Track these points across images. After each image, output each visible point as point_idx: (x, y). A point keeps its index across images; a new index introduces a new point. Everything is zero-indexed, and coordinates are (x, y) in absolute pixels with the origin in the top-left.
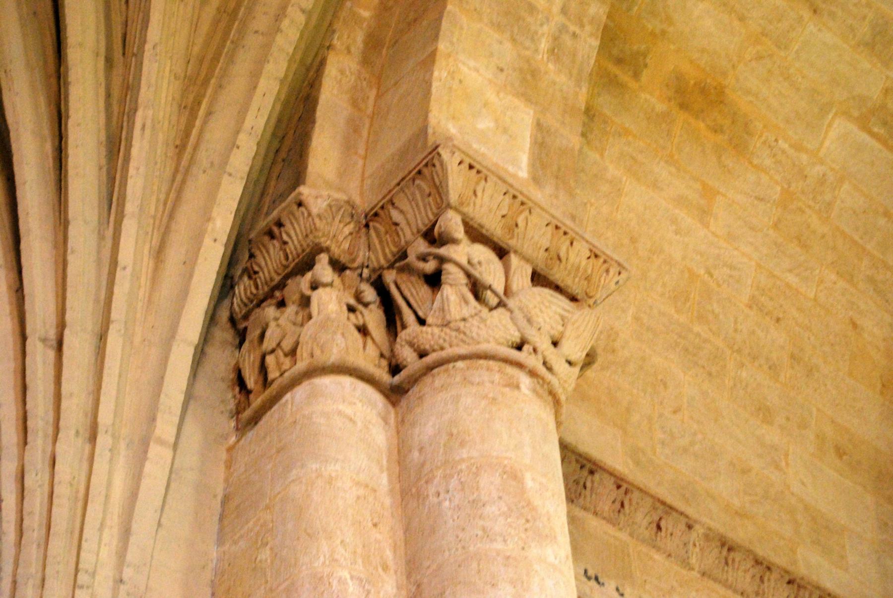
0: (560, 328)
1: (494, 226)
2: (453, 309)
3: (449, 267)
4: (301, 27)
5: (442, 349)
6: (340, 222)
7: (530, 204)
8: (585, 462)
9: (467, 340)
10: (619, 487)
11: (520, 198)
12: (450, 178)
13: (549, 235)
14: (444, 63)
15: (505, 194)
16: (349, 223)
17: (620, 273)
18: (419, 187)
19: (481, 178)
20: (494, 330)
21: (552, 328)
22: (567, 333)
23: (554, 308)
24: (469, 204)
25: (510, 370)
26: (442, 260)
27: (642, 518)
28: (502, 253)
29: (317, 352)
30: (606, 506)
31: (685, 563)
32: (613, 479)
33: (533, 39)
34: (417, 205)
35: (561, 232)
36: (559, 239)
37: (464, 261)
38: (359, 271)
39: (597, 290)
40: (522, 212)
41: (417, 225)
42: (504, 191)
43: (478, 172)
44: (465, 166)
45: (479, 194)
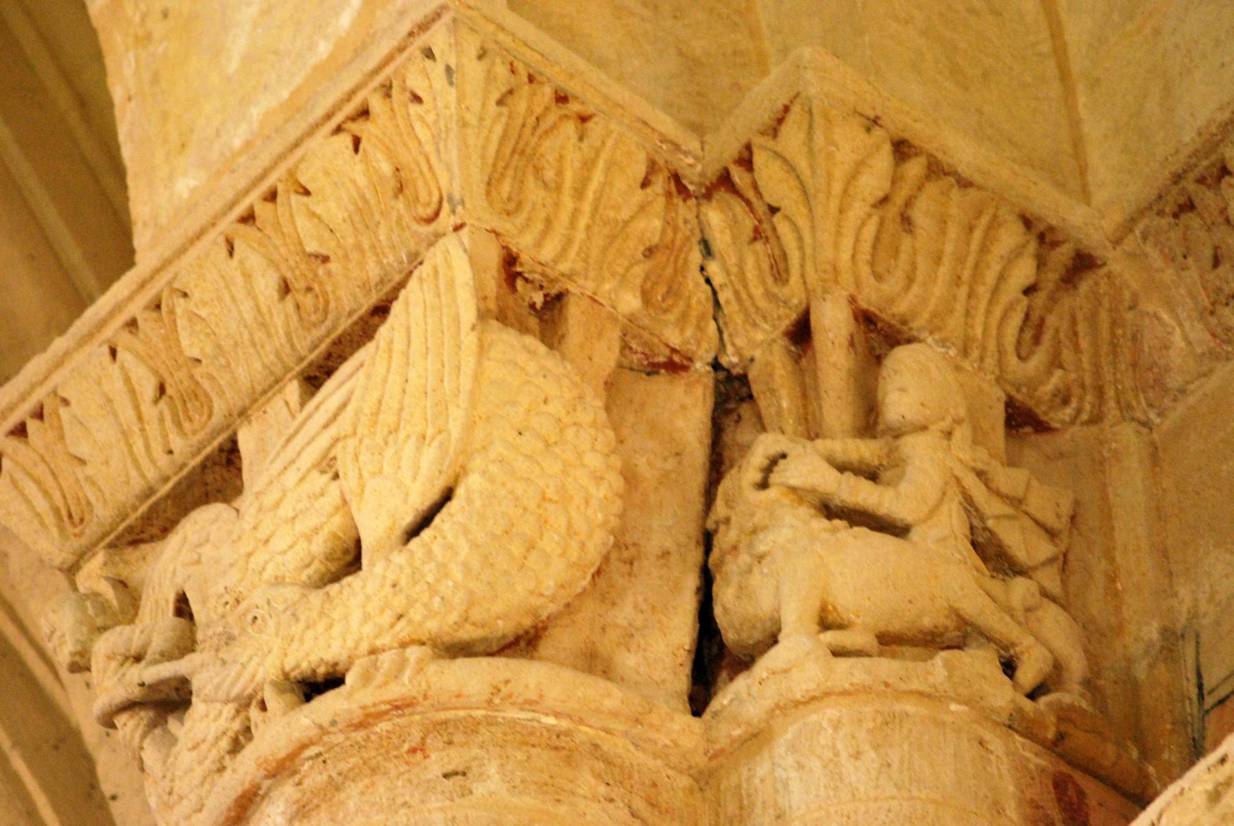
11: (254, 198)
15: (113, 352)
17: (429, 54)
23: (291, 477)
36: (277, 225)
43: (39, 415)
45: (83, 450)
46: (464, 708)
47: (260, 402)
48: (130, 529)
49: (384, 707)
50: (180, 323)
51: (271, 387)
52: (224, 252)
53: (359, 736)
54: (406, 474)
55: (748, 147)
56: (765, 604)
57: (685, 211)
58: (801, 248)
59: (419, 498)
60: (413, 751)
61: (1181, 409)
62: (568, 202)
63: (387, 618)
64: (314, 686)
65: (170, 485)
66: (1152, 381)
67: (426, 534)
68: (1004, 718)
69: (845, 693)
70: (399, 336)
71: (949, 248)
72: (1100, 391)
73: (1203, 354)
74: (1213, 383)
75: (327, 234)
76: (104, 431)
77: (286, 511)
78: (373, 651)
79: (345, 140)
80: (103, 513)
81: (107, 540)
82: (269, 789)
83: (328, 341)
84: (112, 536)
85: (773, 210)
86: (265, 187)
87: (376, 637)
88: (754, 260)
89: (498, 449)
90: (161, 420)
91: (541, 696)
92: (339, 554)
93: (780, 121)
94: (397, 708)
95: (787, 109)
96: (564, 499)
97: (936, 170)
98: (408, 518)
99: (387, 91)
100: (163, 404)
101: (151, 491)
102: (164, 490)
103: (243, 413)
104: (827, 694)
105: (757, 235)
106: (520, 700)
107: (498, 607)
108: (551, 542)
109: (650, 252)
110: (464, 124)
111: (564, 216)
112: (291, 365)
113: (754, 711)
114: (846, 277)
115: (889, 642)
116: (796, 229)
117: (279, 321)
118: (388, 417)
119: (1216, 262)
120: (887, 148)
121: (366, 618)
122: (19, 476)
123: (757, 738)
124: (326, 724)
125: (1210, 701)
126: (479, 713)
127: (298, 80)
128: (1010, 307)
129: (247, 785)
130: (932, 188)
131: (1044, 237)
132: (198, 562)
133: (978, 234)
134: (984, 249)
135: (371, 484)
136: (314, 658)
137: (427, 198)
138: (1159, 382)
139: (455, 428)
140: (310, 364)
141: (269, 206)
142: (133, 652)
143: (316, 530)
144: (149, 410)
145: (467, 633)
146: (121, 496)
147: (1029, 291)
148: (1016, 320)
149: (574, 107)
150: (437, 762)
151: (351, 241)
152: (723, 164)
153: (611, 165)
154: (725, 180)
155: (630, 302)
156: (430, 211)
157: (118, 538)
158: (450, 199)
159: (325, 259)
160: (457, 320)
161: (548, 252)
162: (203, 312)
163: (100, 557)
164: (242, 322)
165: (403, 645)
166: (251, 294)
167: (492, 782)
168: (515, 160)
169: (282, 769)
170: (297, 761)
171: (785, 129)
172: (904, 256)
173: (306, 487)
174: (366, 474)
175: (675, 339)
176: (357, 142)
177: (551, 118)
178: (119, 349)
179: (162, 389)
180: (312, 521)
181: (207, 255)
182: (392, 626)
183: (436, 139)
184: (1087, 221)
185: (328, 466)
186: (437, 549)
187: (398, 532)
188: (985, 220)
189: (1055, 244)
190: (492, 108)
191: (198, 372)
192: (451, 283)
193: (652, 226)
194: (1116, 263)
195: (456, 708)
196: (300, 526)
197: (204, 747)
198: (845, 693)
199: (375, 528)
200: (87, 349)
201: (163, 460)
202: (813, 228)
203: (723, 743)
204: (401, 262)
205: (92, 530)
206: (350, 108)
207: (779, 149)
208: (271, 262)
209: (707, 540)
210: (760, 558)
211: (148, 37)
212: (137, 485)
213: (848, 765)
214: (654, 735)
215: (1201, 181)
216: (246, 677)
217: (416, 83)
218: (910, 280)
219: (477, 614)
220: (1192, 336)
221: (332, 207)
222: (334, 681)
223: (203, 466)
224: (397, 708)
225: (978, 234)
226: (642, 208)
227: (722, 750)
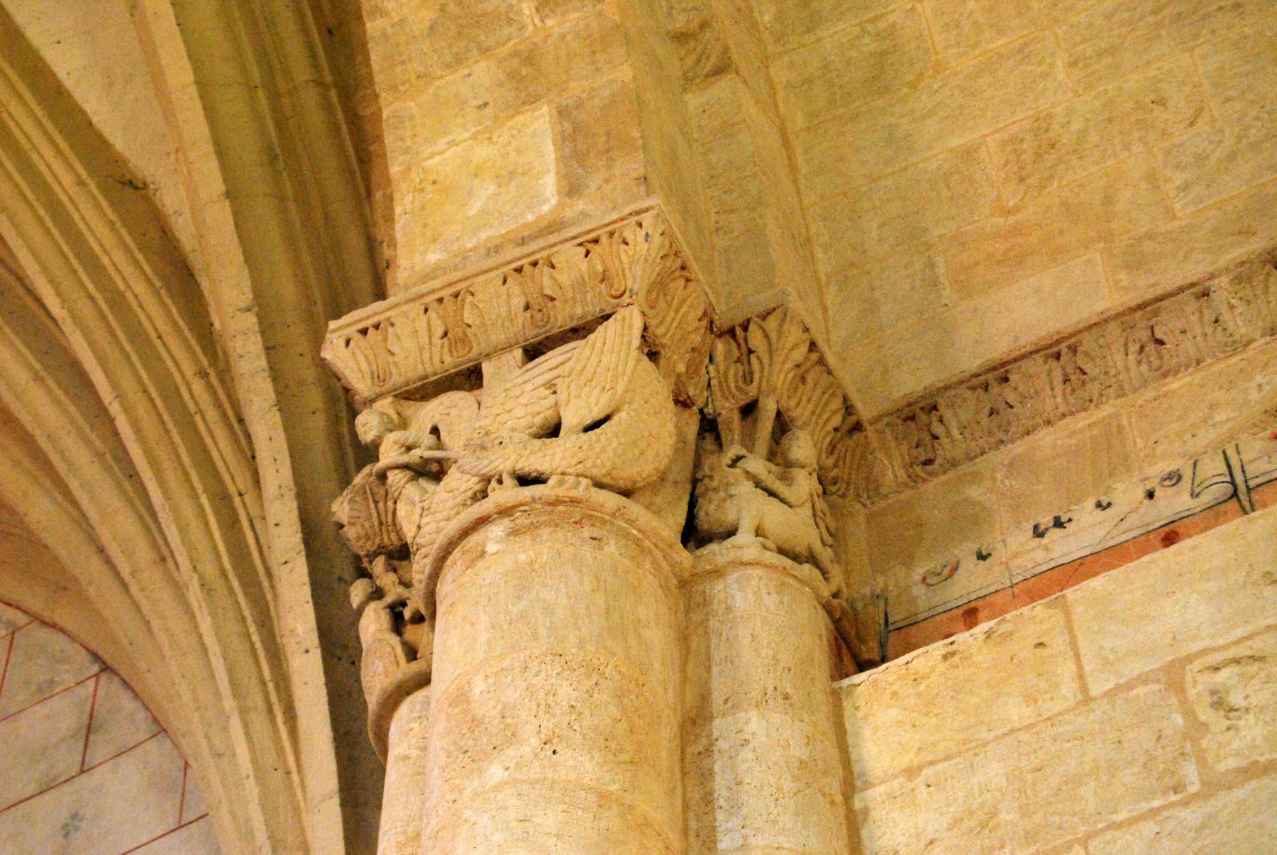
4: (257, 328)
7: (464, 285)
8: (1055, 349)
10: (1058, 356)
11: (446, 293)
14: (404, 186)
15: (426, 310)
17: (640, 225)
23: (529, 387)
27: (1119, 358)
30: (1055, 400)
31: (1237, 345)
32: (1039, 358)
33: (510, 21)
36: (532, 278)
42: (423, 308)
43: (377, 327)
45: (395, 349)
48: (407, 392)
50: (467, 307)
52: (501, 282)
53: (549, 508)
54: (593, 400)
55: (748, 321)
56: (731, 517)
57: (709, 338)
58: (762, 372)
59: (597, 414)
60: (576, 523)
61: (883, 504)
62: (672, 314)
63: (574, 461)
64: (524, 480)
66: (873, 488)
67: (598, 431)
68: (824, 601)
69: (766, 566)
70: (600, 340)
71: (814, 398)
72: (848, 484)
74: (902, 497)
76: (409, 343)
77: (523, 400)
78: (563, 474)
79: (582, 250)
80: (397, 379)
85: (750, 352)
86: (532, 259)
88: (735, 371)
89: (635, 405)
90: (442, 347)
93: (769, 314)
95: (774, 309)
96: (658, 439)
97: (821, 361)
98: (588, 421)
99: (611, 234)
100: (445, 340)
101: (426, 377)
102: (431, 379)
103: (488, 356)
104: (757, 564)
105: (738, 360)
107: (623, 475)
108: (650, 454)
109: (693, 349)
110: (646, 261)
111: (669, 319)
113: (720, 560)
114: (778, 391)
115: (781, 551)
116: (761, 363)
117: (520, 320)
118: (588, 374)
119: (917, 446)
120: (808, 344)
121: (563, 459)
122: (357, 351)
123: (717, 573)
125: (891, 627)
126: (607, 517)
127: (512, 227)
128: (828, 433)
130: (818, 368)
131: (848, 409)
132: (448, 414)
133: (826, 396)
134: (826, 404)
135: (574, 401)
136: (533, 468)
137: (618, 287)
138: (876, 489)
139: (620, 388)
143: (538, 414)
144: (437, 342)
145: (607, 480)
147: (836, 430)
148: (828, 440)
149: (686, 273)
150: (586, 532)
151: (570, 295)
153: (692, 306)
154: (731, 332)
155: (681, 368)
158: (631, 291)
159: (553, 299)
160: (630, 343)
161: (659, 332)
162: (481, 305)
163: (390, 399)
164: (499, 315)
165: (578, 475)
166: (508, 304)
167: (611, 548)
168: (659, 286)
169: (505, 512)
171: (771, 318)
172: (799, 393)
173: (537, 393)
175: (691, 392)
177: (677, 274)
179: (446, 334)
180: (537, 409)
183: (631, 263)
184: (865, 411)
185: (552, 387)
186: (603, 438)
188: (830, 391)
189: (851, 414)
190: (658, 260)
191: (468, 331)
192: (631, 327)
193: (697, 339)
194: (870, 431)
196: (529, 409)
197: (456, 493)
198: (766, 566)
199: (571, 419)
200: (412, 305)
201: (437, 365)
202: (771, 365)
203: (700, 569)
205: (389, 385)
206: (591, 236)
208: (524, 293)
209: (695, 482)
210: (731, 496)
211: (422, 190)
212: (420, 372)
213: (765, 597)
214: (675, 555)
215: (922, 409)
216: (492, 466)
217: (628, 235)
218: (798, 404)
219: (614, 473)
220: (898, 474)
221: (565, 278)
222: (539, 480)
223: (457, 374)
225: (826, 396)
226: (697, 329)
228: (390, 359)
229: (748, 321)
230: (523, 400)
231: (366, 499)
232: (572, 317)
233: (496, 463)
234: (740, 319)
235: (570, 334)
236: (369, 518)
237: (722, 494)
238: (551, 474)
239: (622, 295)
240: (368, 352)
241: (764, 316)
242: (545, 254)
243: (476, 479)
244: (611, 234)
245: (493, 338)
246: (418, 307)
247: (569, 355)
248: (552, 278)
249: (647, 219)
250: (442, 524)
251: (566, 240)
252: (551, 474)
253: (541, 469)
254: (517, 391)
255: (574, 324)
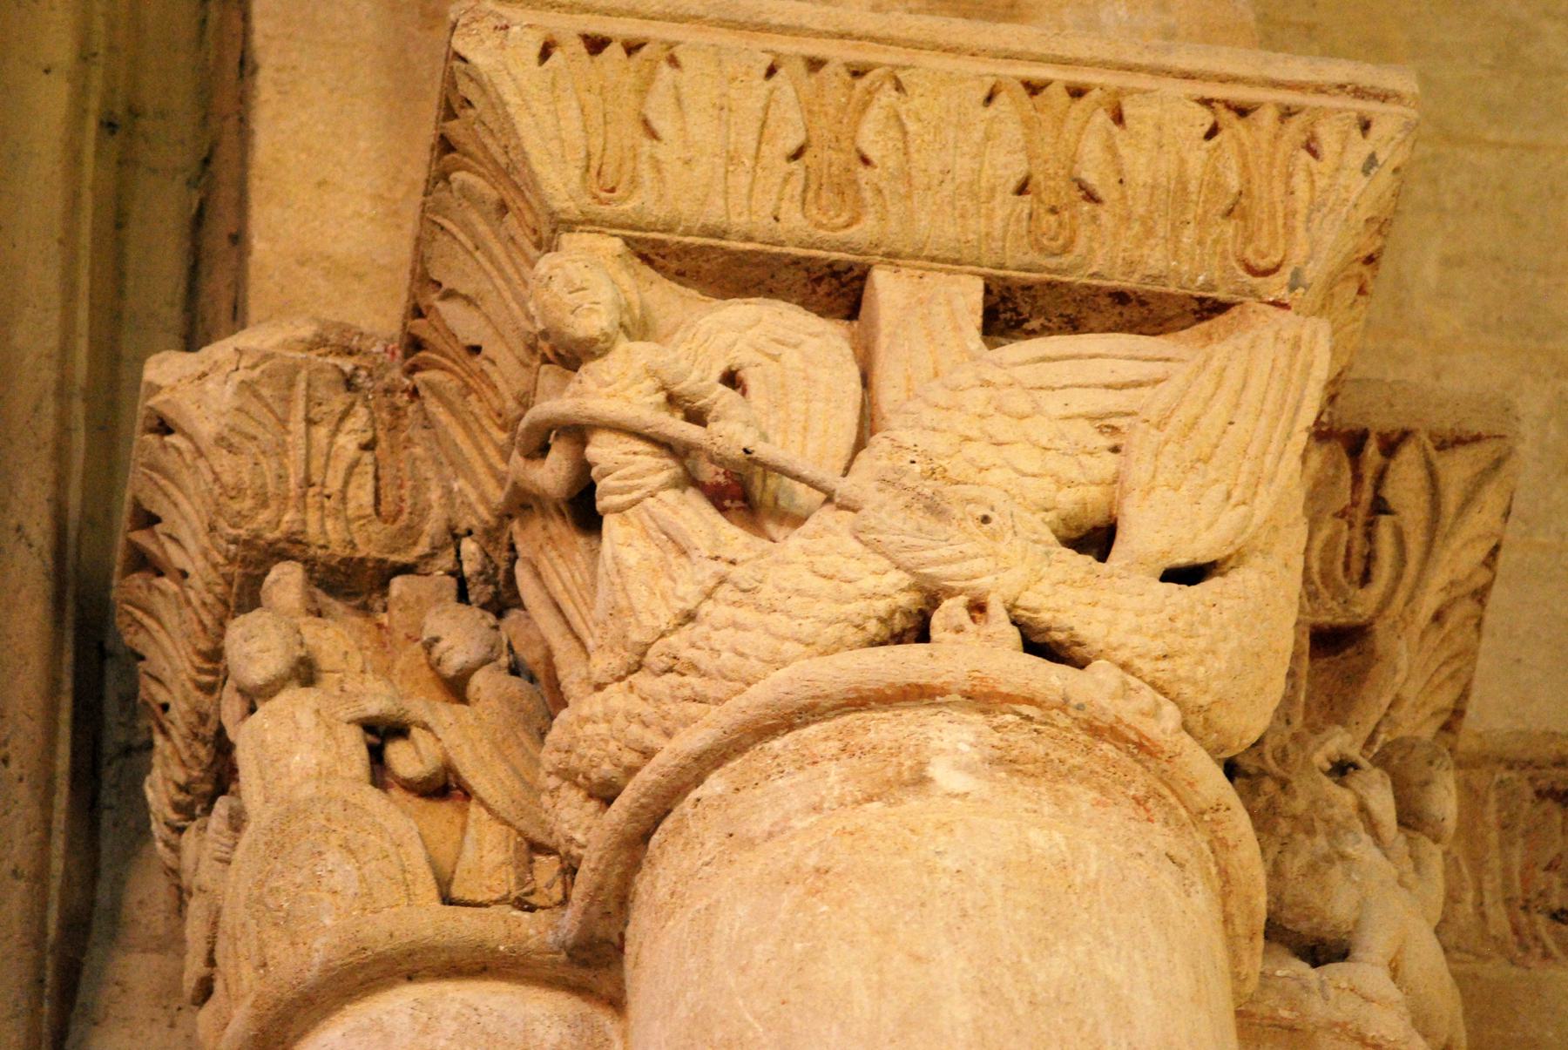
0: (1107, 465)
1: (767, 209)
2: (639, 595)
3: (602, 450)
5: (647, 754)
6: (310, 422)
9: (710, 688)
11: (838, 53)
12: (524, 123)
13: (1012, 131)
15: (771, 72)
16: (346, 414)
17: (1365, 126)
18: (465, 191)
19: (654, 64)
20: (800, 599)
21: (1061, 483)
22: (1139, 473)
23: (1053, 404)
24: (634, 182)
25: (882, 727)
26: (578, 432)
28: (839, 290)
29: (279, 950)
34: (492, 259)
35: (1057, 96)
36: (1061, 121)
37: (643, 407)
38: (446, 561)
39: (1290, 230)
40: (865, 106)
41: (436, 350)
42: (767, 60)
43: (632, 48)
44: (571, 51)
45: (662, 125)
46: (1179, 798)
47: (919, 263)
49: (1133, 736)
50: (875, 113)
51: (945, 261)
55: (1405, 435)
63: (1158, 647)
65: (749, 246)
73: (1495, 938)
75: (1114, 180)
77: (1040, 430)
79: (1205, 118)
80: (643, 203)
81: (628, 233)
82: (954, 702)
83: (1047, 276)
84: (637, 234)
87: (1140, 656)
91: (1235, 846)
92: (1073, 524)
94: (1140, 746)
95: (1477, 439)
98: (1182, 560)
99: (1287, 113)
101: (723, 234)
103: (892, 257)
106: (1220, 834)
112: (985, 261)
124: (1073, 702)
129: (937, 682)
136: (1066, 619)
140: (1004, 279)
141: (1066, 98)
142: (677, 389)
143: (1071, 484)
146: (686, 208)
149: (1366, 271)
151: (1140, 210)
152: (1367, 425)
156: (1264, 264)
157: (637, 240)
158: (1296, 274)
159: (1091, 197)
162: (912, 127)
170: (1005, 706)
174: (1160, 479)
176: (1212, 133)
178: (781, 71)
179: (797, 155)
181: (962, 80)
182: (1157, 659)
183: (1314, 207)
187: (1167, 563)
191: (863, 173)
192: (1308, 366)
195: (1173, 791)
196: (1054, 462)
199: (1149, 535)
204: (1193, 281)
207: (1438, 464)
210: (1343, 857)
216: (953, 569)
223: (796, 262)
224: (1140, 746)
227: (1252, 1015)
228: (647, 145)
229: (1405, 435)
230: (1040, 430)
231: (287, 400)
232: (1131, 267)
233: (977, 565)
234: (1382, 422)
235: (1104, 302)
236: (281, 449)
237: (1321, 842)
238: (1100, 654)
239: (1266, 273)
240: (591, 99)
241: (1450, 442)
242: (1112, 80)
243: (905, 579)
244: (1287, 113)
245: (923, 221)
246: (759, 51)
247: (1158, 369)
248: (1111, 149)
249: (1388, 120)
250: (790, 648)
251: (1168, 73)
252: (1100, 654)
253: (1083, 632)
254: (1020, 403)
255: (1130, 284)
